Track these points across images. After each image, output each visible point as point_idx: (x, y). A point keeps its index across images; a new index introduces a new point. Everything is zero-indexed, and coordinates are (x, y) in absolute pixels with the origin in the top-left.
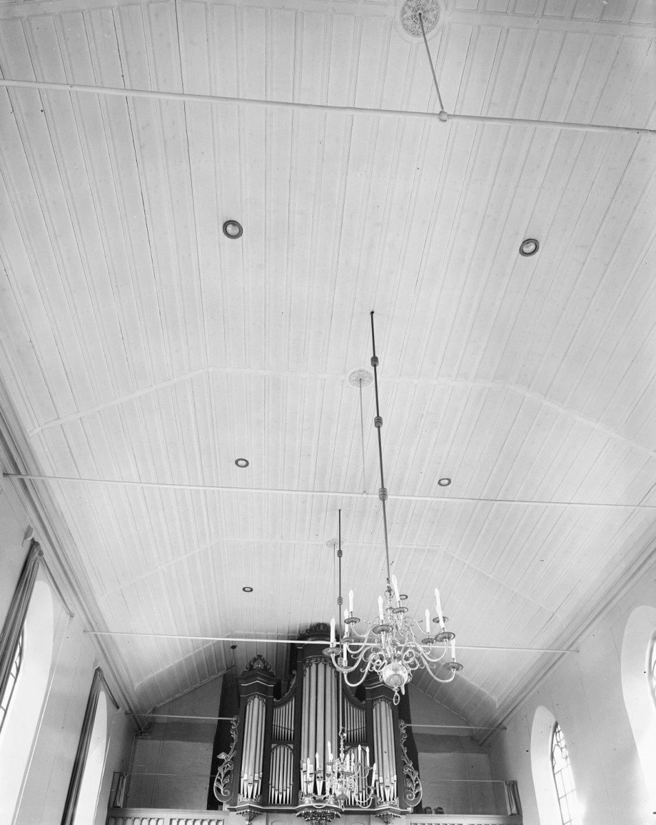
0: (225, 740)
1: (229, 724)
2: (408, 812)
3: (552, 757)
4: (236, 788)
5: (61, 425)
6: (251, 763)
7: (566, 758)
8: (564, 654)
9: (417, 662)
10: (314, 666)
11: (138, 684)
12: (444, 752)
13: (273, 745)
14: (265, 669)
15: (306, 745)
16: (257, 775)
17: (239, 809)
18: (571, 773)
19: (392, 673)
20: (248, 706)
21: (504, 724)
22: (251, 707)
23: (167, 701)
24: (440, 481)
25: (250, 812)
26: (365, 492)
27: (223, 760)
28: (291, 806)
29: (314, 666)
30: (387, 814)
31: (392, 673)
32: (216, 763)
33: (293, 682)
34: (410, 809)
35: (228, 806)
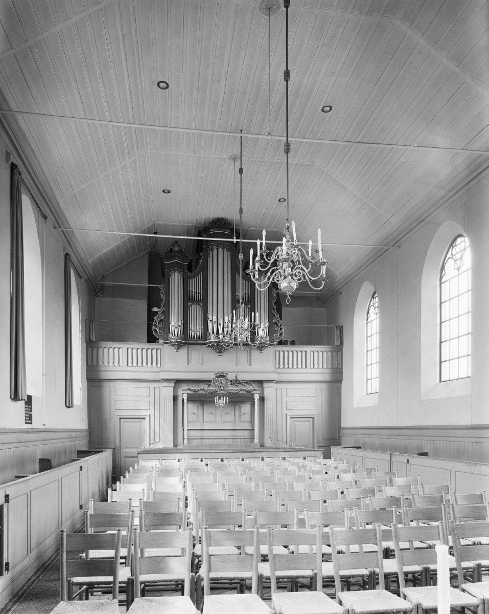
0: (155, 299)
1: (158, 289)
2: (274, 345)
3: (368, 313)
4: (167, 330)
5: (14, 54)
6: (175, 316)
7: (377, 314)
8: (388, 249)
9: (302, 277)
10: (215, 251)
11: (91, 260)
12: (299, 307)
13: (189, 304)
14: (181, 252)
15: (211, 302)
16: (180, 322)
17: (171, 342)
18: (378, 340)
19: (287, 284)
20: (170, 278)
21: (341, 290)
22: (173, 279)
23: (111, 271)
24: (323, 108)
25: (178, 344)
26: (269, 134)
27: (157, 312)
28: (202, 341)
29: (215, 251)
30: (262, 346)
31: (287, 284)
32: (151, 316)
33: (201, 261)
34: (276, 343)
35: (163, 341)
